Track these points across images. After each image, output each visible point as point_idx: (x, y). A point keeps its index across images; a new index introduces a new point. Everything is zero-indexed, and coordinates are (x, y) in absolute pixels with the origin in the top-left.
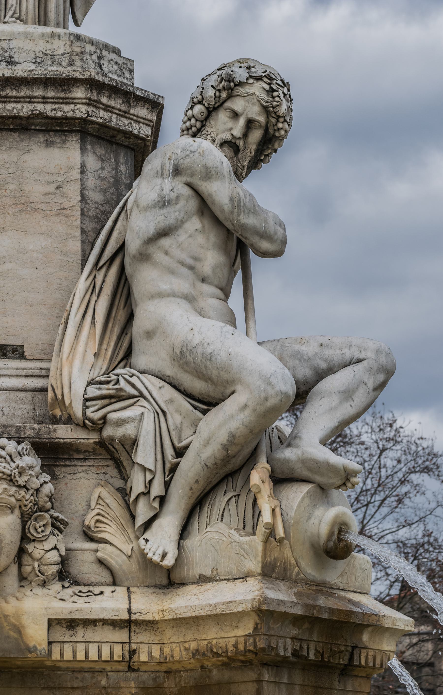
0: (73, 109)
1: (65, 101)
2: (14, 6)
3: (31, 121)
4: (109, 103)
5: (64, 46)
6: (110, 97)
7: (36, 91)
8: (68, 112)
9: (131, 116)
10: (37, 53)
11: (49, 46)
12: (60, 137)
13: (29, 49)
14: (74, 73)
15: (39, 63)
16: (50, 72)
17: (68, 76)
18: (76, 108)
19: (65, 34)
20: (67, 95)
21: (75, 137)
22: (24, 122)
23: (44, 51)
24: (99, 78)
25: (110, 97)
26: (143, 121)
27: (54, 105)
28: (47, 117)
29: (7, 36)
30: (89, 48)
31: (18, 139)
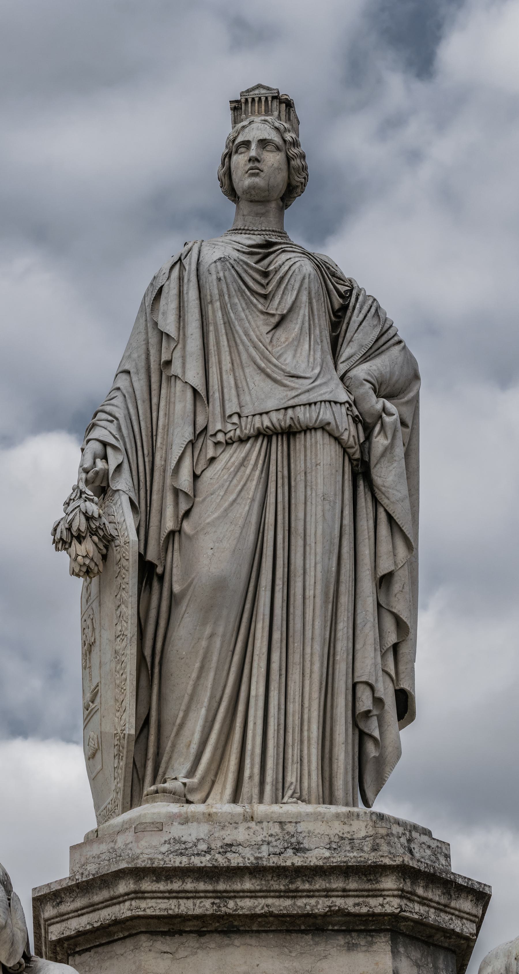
0: (381, 903)
1: (371, 893)
2: (294, 784)
3: (329, 919)
4: (425, 895)
5: (366, 827)
6: (426, 887)
7: (334, 883)
8: (375, 907)
9: (452, 911)
10: (332, 837)
11: (347, 828)
12: (365, 938)
13: (321, 832)
14: (382, 859)
15: (335, 849)
16: (351, 858)
17: (375, 863)
18: (385, 901)
19: (365, 813)
20: (374, 887)
21: (385, 937)
22: (319, 921)
23: (341, 835)
24: (413, 864)
25: (426, 887)
26: (466, 916)
27: (357, 899)
28: (349, 914)
29: (292, 818)
30: (396, 829)
31: (311, 942)
